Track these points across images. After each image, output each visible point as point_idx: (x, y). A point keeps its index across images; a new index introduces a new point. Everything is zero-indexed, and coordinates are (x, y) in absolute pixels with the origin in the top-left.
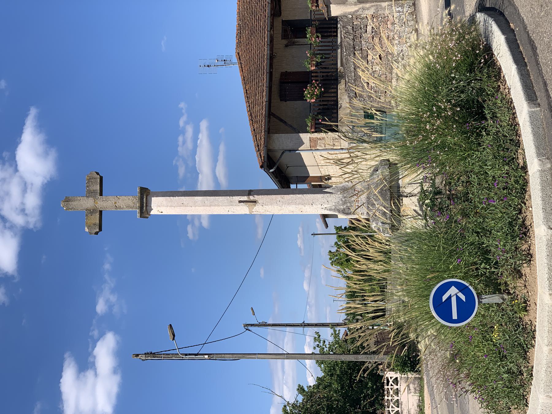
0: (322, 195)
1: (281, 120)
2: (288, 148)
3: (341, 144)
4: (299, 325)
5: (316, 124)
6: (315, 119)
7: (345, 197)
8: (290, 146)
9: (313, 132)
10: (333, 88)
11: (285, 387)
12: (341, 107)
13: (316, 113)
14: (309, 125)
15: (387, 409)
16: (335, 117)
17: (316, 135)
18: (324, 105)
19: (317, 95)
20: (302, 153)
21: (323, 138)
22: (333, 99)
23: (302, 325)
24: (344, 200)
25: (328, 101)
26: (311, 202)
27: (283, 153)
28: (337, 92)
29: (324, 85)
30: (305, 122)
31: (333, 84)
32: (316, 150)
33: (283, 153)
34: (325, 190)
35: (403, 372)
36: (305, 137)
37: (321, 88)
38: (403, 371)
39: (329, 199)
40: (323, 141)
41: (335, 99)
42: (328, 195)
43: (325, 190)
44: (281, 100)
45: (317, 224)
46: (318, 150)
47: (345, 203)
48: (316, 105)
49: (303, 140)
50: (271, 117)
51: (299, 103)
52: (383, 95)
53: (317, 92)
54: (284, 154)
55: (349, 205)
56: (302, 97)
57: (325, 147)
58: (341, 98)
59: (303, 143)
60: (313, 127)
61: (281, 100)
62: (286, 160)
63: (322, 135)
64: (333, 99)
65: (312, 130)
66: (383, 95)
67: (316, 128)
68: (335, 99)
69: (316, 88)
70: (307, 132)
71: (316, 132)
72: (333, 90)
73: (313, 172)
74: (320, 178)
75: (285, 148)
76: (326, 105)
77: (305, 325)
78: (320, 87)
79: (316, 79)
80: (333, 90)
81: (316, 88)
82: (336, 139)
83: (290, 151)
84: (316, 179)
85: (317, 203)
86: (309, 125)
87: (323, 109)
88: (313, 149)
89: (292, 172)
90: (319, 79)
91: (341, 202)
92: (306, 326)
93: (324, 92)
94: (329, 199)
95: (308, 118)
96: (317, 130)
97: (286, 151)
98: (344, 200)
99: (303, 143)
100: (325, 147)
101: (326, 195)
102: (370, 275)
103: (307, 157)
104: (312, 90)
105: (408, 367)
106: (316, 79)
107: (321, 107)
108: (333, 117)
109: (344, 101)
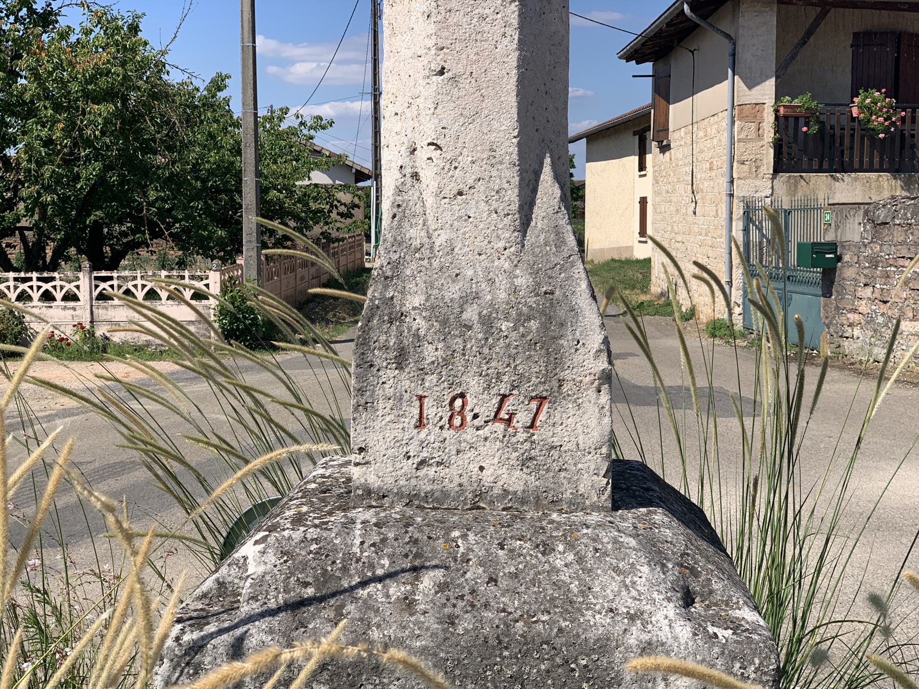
0: (509, 149)
1: (809, 33)
2: (739, 50)
3: (745, 178)
4: (375, 84)
5: (797, 118)
6: (809, 116)
7: (487, 322)
8: (745, 55)
9: (776, 111)
10: (882, 160)
11: (315, 65)
12: (836, 179)
13: (822, 118)
14: (796, 102)
15: (139, 275)
16: (811, 165)
17: (769, 118)
18: (842, 137)
19: (869, 121)
20: (726, 84)
21: (760, 137)
22: (856, 160)
23: (375, 90)
24: (471, 314)
25: (852, 148)
26: (455, 68)
27: (728, 36)
28: (871, 170)
29: (891, 137)
30: (802, 93)
31: (892, 160)
32: (733, 117)
33: (728, 36)
34: (547, 174)
35: (220, 313)
36: (766, 91)
37: (886, 130)
38: (223, 312)
39: (477, 206)
40: (753, 135)
41: (856, 166)
42: (512, 195)
43: (547, 174)
44: (856, 35)
45: (587, 122)
46: (733, 123)
47: (447, 321)
48: (844, 121)
49: (758, 88)
50: (819, 9)
51: (846, 79)
52: (877, 295)
53: (877, 121)
54: (727, 41)
55: (431, 353)
56: (859, 84)
57: (740, 140)
58: (856, 179)
59: (750, 87)
60: (790, 112)
61: (856, 35)
62: (710, 45)
63: (769, 134)
64: (856, 160)
65: (782, 110)
66: (877, 295)
67: (786, 117)
68: (856, 166)
69: (886, 120)
70: (778, 98)
71: (777, 118)
72: (876, 160)
73: (678, 112)
74: (664, 130)
75: (740, 43)
76: (841, 144)
77: (375, 96)
78: (888, 127)
79: (908, 120)
80: (876, 160)
81: (886, 120)
82: (757, 168)
83: (734, 55)
84: (662, 120)
85: (447, 114)
86: (796, 102)
87: (833, 136)
88: (736, 112)
89: (680, 64)
90: (907, 127)
91: (453, 291)
92: (375, 99)
93: (873, 139)
94: (477, 206)
95: (813, 98)
96: (782, 121)
97: (734, 44)
98: (471, 314)
99: (750, 87)
100: (740, 140)
101: (508, 178)
102: (177, 364)
103: (715, 98)
104: (881, 110)
105: (231, 323)
106: (908, 120)
107: (838, 132)
108: (811, 160)
109: (850, 188)
